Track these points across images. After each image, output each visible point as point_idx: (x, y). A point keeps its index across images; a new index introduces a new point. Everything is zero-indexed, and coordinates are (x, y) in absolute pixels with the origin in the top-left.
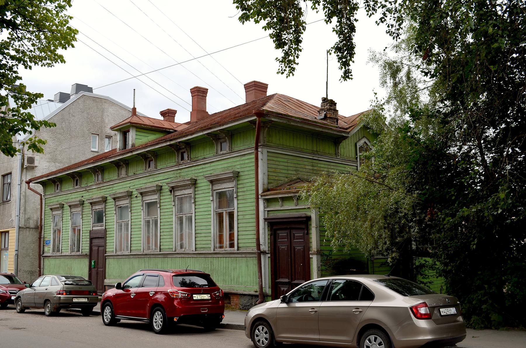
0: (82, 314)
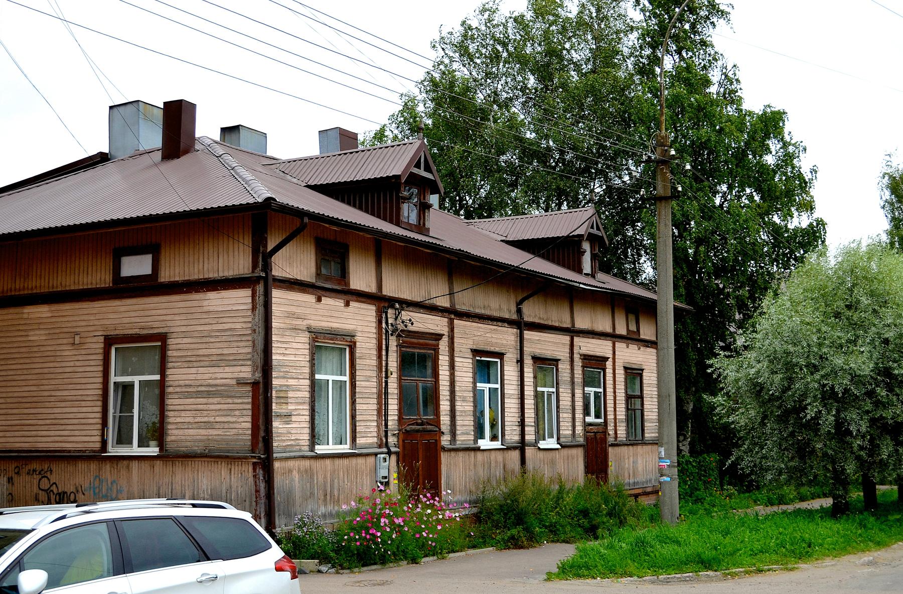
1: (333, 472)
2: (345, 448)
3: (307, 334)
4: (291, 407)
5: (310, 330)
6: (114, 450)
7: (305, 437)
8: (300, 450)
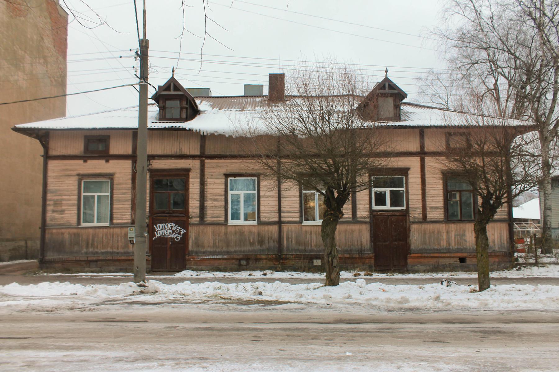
1: (226, 234)
2: (107, 224)
4: (64, 208)
5: (78, 175)
6: (83, 225)
7: (74, 220)
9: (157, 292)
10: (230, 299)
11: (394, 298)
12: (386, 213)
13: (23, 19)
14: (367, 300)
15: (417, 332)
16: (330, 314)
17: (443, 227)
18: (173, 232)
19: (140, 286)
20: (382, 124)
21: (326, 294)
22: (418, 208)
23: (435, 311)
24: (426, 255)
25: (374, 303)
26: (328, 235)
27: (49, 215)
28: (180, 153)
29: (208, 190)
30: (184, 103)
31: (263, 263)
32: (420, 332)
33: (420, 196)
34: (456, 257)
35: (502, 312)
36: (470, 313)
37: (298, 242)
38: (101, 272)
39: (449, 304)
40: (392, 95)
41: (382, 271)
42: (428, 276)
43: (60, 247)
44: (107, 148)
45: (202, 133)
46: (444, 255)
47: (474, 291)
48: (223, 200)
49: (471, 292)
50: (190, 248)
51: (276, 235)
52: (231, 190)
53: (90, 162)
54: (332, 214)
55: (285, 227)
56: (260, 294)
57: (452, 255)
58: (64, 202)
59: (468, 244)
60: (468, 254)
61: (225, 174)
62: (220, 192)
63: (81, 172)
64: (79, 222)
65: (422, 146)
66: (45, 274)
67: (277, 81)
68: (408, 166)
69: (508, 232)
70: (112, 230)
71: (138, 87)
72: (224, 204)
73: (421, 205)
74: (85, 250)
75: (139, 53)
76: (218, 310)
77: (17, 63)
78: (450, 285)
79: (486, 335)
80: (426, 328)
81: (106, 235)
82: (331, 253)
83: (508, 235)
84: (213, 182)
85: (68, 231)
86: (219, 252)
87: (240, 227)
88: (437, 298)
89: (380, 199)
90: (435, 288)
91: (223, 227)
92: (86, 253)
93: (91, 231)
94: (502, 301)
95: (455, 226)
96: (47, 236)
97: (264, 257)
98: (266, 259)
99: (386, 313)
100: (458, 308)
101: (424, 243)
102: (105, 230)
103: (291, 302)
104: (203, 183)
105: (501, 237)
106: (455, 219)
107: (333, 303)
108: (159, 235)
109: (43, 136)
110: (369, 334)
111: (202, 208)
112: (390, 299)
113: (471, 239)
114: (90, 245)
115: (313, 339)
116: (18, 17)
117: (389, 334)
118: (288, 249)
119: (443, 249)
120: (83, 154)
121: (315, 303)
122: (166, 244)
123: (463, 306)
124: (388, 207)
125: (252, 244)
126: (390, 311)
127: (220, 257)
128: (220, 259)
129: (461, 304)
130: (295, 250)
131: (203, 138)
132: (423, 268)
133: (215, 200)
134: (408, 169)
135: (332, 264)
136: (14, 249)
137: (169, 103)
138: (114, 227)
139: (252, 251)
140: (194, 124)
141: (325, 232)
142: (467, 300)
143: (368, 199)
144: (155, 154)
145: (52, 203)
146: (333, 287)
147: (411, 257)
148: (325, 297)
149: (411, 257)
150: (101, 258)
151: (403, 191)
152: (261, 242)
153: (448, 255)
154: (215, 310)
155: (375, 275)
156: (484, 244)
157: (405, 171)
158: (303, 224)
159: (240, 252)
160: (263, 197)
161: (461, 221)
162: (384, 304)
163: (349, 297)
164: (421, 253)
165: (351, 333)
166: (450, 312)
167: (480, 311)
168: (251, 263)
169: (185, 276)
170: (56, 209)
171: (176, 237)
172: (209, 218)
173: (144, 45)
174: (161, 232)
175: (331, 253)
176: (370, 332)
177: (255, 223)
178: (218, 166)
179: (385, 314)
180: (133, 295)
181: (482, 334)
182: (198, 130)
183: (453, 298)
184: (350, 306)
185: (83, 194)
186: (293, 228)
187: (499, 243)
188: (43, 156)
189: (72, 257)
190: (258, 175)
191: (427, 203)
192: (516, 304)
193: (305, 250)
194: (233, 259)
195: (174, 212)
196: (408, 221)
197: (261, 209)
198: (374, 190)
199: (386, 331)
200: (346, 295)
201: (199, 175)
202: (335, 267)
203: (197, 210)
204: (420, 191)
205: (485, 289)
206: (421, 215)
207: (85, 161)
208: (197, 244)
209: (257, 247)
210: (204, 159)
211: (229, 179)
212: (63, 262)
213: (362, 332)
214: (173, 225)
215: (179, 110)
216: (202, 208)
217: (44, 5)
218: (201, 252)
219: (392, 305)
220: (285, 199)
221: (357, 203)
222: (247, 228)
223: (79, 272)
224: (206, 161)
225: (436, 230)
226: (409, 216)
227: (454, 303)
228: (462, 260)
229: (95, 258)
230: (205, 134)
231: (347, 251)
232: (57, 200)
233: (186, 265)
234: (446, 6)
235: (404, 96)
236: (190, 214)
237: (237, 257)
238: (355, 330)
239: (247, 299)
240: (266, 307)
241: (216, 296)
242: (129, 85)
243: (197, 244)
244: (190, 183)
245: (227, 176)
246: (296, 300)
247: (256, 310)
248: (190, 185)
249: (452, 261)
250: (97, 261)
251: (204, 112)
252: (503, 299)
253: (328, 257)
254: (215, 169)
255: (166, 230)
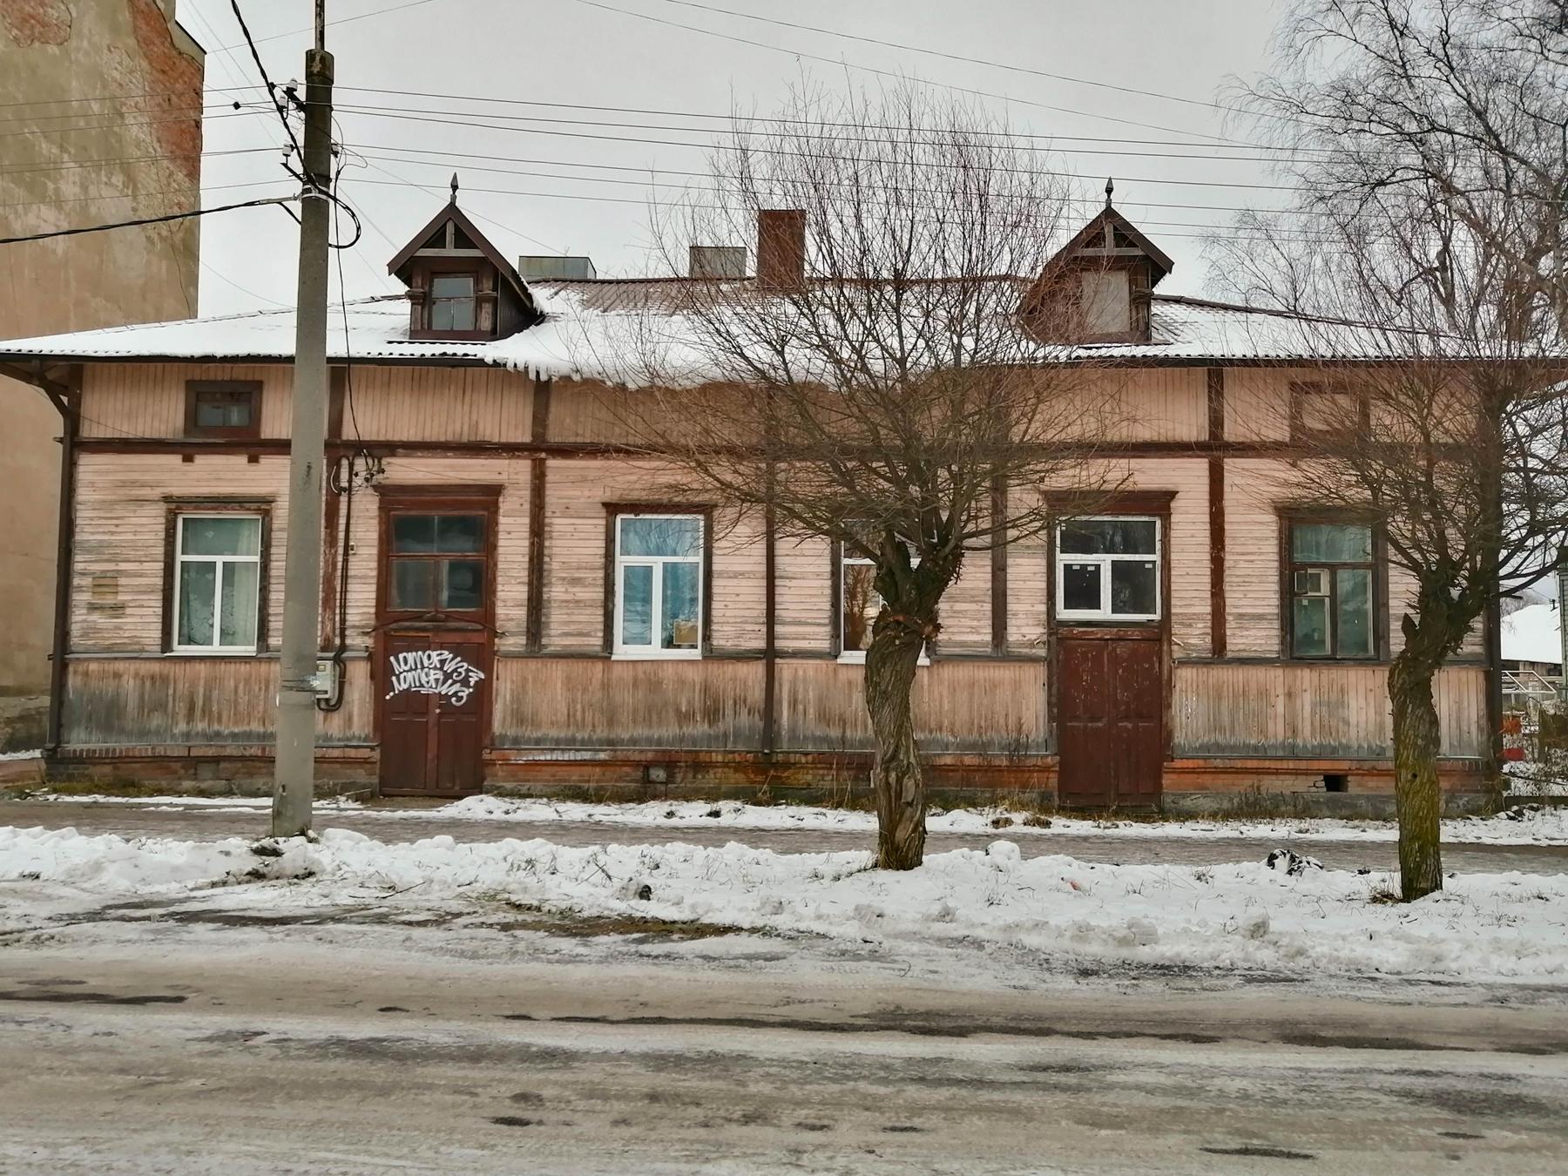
0: (1478, 624)
1: (606, 686)
2: (251, 650)
3: (163, 506)
4: (121, 597)
5: (167, 499)
6: (180, 650)
7: (154, 634)
8: (143, 651)
9: (311, 874)
10: (539, 909)
11: (1104, 924)
12: (1099, 633)
13: (53, 49)
14: (1008, 928)
15: (1179, 1091)
16: (866, 984)
17: (1275, 677)
18: (447, 676)
19: (261, 852)
20: (1093, 352)
21: (864, 901)
22: (1197, 617)
23: (1250, 980)
24: (1218, 763)
25: (1032, 940)
26: (885, 695)
27: (79, 618)
28: (473, 439)
29: (555, 550)
30: (487, 288)
31: (710, 780)
32: (1191, 1093)
33: (1206, 580)
34: (1316, 773)
35: (1500, 993)
36: (1378, 995)
37: (824, 717)
38: (229, 793)
39: (1301, 952)
40: (1118, 264)
41: (1082, 812)
42: (1226, 830)
43: (108, 715)
44: (255, 418)
45: (532, 376)
46: (1278, 765)
47: (1382, 898)
48: (601, 582)
49: (1374, 900)
50: (497, 728)
51: (757, 694)
52: (626, 552)
53: (201, 460)
54: (898, 623)
55: (785, 668)
56: (645, 893)
57: (1303, 765)
58: (122, 581)
59: (1353, 732)
60: (1354, 765)
61: (605, 505)
62: (591, 559)
63: (176, 491)
64: (166, 643)
65: (1216, 422)
66: (52, 797)
67: (781, 231)
68: (1171, 487)
69: (1482, 697)
70: (264, 667)
71: (296, 207)
72: (601, 596)
73: (1209, 609)
74: (182, 727)
75: (301, 94)
76: (474, 956)
77: (34, 177)
78: (1300, 870)
79: (1467, 1123)
80: (1214, 1072)
81: (247, 681)
82: (894, 757)
83: (1483, 706)
84: (571, 528)
85: (133, 666)
86: (583, 742)
87: (648, 667)
88: (1259, 930)
89: (1082, 589)
90: (1249, 878)
91: (599, 666)
92: (187, 736)
93: (202, 668)
94: (1497, 946)
95: (1315, 674)
96: (73, 681)
97: (720, 758)
98: (725, 765)
99: (1067, 983)
100: (1333, 969)
101: (1217, 727)
102: (244, 668)
103: (740, 929)
104: (538, 531)
105: (1459, 711)
106: (1314, 653)
107: (887, 936)
108: (404, 686)
109: (64, 379)
110: (985, 1096)
111: (536, 605)
112: (1089, 928)
113: (1363, 718)
114: (198, 712)
115: (747, 1120)
116: (37, 44)
117: (1062, 1098)
118: (793, 737)
119: (1274, 747)
120: (180, 437)
121: (824, 936)
122: (425, 713)
123: (1351, 961)
124: (1105, 613)
125: (684, 717)
126: (1085, 973)
127: (587, 756)
128: (583, 763)
129: (1344, 953)
130: (817, 740)
131: (543, 390)
132: (1207, 804)
133: (575, 581)
134: (1171, 495)
135: (899, 795)
136: (21, 718)
137: (442, 286)
138: (270, 659)
139: (682, 739)
140: (517, 350)
141: (878, 684)
142: (1364, 939)
143: (1044, 585)
144: (396, 438)
145: (88, 581)
146: (902, 875)
147: (1174, 771)
148: (860, 913)
149: (1174, 771)
150: (228, 752)
151: (1154, 562)
152: (713, 713)
153: (1291, 765)
154: (462, 954)
155: (1060, 825)
156: (1425, 738)
157: (1160, 502)
158: (839, 661)
159: (649, 741)
160: (721, 574)
161: (1332, 660)
162: (1066, 943)
163: (946, 915)
164: (1205, 759)
165: (912, 1091)
166: (1304, 988)
167: (1418, 982)
168: (679, 777)
169: (469, 815)
170: (97, 601)
171: (455, 694)
172: (555, 638)
173: (320, 69)
174: (410, 675)
175: (894, 757)
176: (992, 1085)
177: (696, 654)
178: (584, 480)
179: (1065, 991)
180: (224, 883)
181: (1444, 1114)
182: (521, 367)
183: (1315, 925)
184: (945, 950)
185: (180, 558)
186: (811, 673)
187: (1455, 732)
188: (61, 441)
189: (142, 747)
190: (706, 509)
191: (1228, 602)
192: (1549, 961)
193: (843, 740)
194: (626, 763)
195: (448, 617)
196: (1166, 658)
197: (714, 613)
198: (1062, 559)
199: (1055, 1078)
200: (936, 909)
201: (527, 506)
202: (910, 804)
203: (521, 613)
204: (1208, 564)
205: (1424, 892)
206: (1208, 639)
207: (188, 459)
208: (519, 718)
209: (701, 728)
210: (543, 455)
211: (619, 518)
212: (116, 760)
213: (959, 1082)
214: (447, 655)
215: (472, 304)
216: (536, 605)
217: (125, 16)
218: (528, 741)
219: (1094, 950)
220: (787, 583)
221: (1009, 599)
222: (670, 671)
223: (161, 792)
224: (552, 463)
225: (1253, 685)
226: (1170, 643)
227: (1320, 949)
228: (1335, 782)
229: (211, 752)
230: (543, 377)
231: (973, 746)
232: (104, 574)
233: (483, 779)
234: (1300, 13)
235: (1158, 266)
236: (498, 624)
237: (637, 757)
238: (932, 1072)
239: (595, 912)
240: (646, 948)
241: (493, 898)
242: (269, 202)
243: (519, 718)
244: (501, 528)
245: (612, 508)
246: (759, 923)
247: (604, 960)
248: (501, 536)
249: (1301, 785)
250: (216, 760)
251: (555, 318)
252: (1497, 940)
253: (887, 771)
254: (578, 487)
255: (424, 671)
